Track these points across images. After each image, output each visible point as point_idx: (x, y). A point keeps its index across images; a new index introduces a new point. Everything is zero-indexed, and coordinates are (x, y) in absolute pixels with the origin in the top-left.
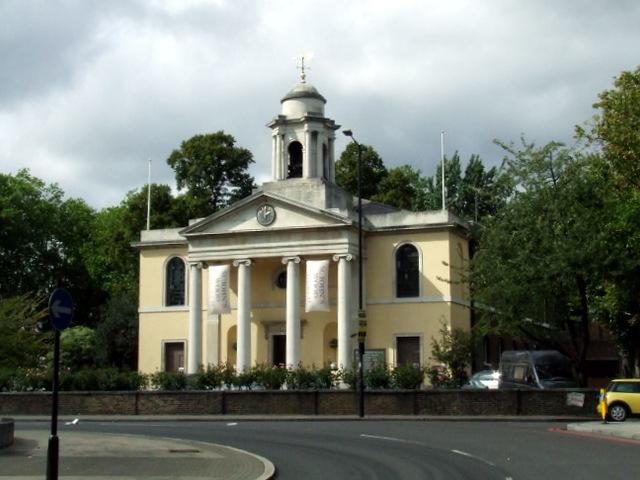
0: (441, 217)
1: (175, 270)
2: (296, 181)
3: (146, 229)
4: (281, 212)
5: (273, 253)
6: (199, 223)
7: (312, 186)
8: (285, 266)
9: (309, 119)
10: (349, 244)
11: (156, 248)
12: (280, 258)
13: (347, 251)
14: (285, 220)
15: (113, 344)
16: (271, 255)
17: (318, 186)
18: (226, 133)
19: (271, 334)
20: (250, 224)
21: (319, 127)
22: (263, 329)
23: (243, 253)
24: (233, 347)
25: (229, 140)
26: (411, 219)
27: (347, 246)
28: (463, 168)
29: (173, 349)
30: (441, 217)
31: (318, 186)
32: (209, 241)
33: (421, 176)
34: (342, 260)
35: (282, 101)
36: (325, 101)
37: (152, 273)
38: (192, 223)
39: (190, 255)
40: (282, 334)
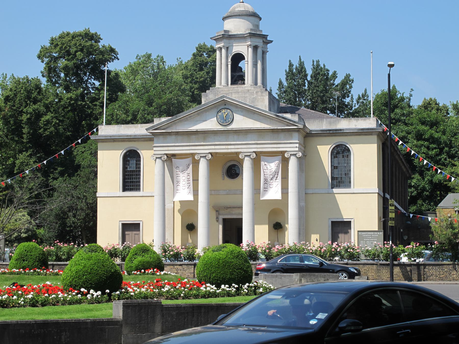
0: (370, 123)
1: (131, 160)
2: (238, 88)
3: (102, 124)
4: (237, 117)
5: (231, 149)
6: (163, 122)
7: (257, 92)
8: (243, 160)
9: (252, 35)
10: (299, 143)
11: (113, 141)
12: (237, 154)
13: (297, 149)
14: (241, 122)
15: (64, 225)
16: (229, 151)
17: (262, 92)
18: (92, 31)
19: (221, 217)
20: (211, 124)
21: (259, 42)
22: (214, 213)
23: (203, 149)
24: (191, 228)
25: (94, 38)
26: (345, 124)
27: (297, 145)
28: (309, 72)
29: (130, 228)
30: (370, 123)
31: (262, 92)
32: (173, 137)
33: (356, 91)
34: (202, 159)
35: (224, 19)
36: (260, 19)
37: (109, 165)
38: (157, 121)
39: (155, 149)
40: (239, 217)
